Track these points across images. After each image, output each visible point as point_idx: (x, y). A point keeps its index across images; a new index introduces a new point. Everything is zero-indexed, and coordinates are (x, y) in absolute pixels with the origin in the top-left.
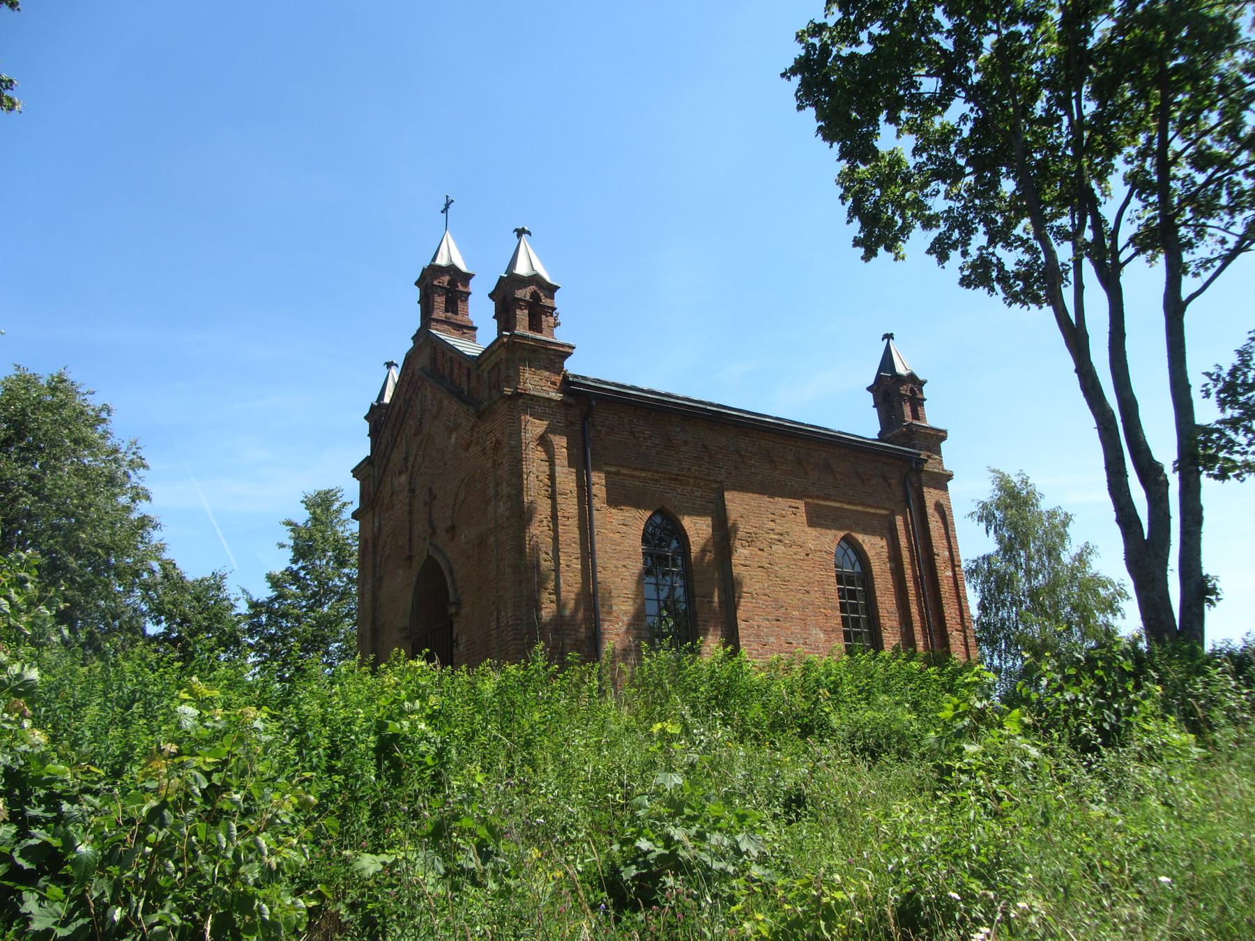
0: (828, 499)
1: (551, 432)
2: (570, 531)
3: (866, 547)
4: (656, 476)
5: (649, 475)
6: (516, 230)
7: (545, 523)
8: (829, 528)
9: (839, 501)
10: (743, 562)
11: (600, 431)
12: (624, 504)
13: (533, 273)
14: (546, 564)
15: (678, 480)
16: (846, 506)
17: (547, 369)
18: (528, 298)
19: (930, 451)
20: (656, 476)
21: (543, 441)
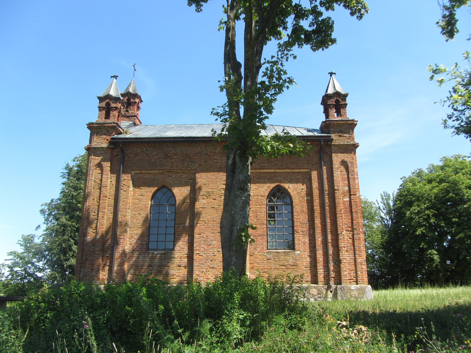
0: (264, 169)
1: (103, 161)
2: (108, 202)
3: (290, 191)
4: (161, 172)
5: (156, 171)
6: (329, 73)
7: (96, 199)
8: (265, 183)
9: (274, 169)
10: (202, 206)
11: (130, 157)
12: (142, 186)
13: (335, 91)
14: (93, 215)
15: (172, 172)
16: (277, 171)
17: (105, 134)
18: (334, 103)
19: (342, 133)
20: (161, 172)
21: (99, 165)
